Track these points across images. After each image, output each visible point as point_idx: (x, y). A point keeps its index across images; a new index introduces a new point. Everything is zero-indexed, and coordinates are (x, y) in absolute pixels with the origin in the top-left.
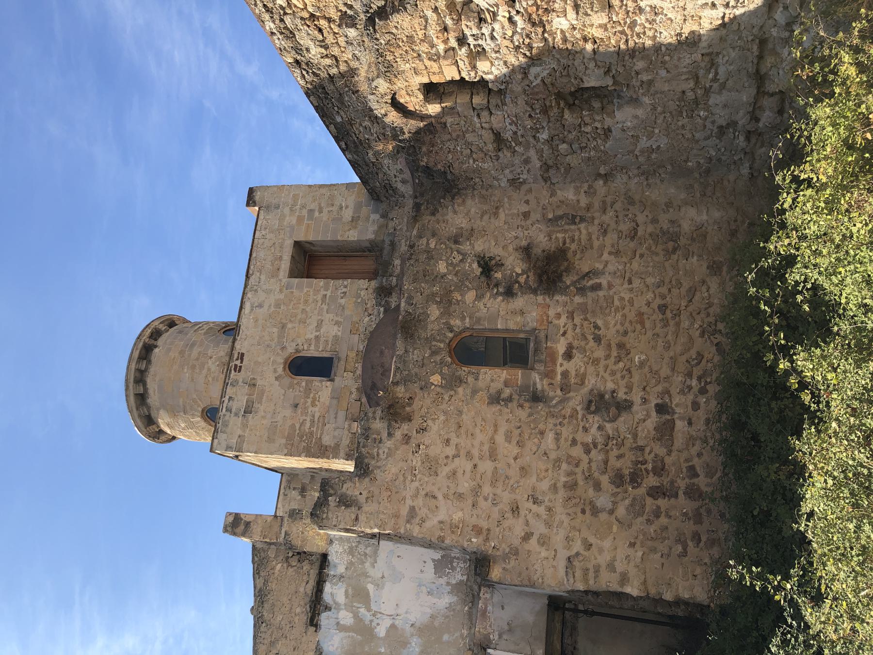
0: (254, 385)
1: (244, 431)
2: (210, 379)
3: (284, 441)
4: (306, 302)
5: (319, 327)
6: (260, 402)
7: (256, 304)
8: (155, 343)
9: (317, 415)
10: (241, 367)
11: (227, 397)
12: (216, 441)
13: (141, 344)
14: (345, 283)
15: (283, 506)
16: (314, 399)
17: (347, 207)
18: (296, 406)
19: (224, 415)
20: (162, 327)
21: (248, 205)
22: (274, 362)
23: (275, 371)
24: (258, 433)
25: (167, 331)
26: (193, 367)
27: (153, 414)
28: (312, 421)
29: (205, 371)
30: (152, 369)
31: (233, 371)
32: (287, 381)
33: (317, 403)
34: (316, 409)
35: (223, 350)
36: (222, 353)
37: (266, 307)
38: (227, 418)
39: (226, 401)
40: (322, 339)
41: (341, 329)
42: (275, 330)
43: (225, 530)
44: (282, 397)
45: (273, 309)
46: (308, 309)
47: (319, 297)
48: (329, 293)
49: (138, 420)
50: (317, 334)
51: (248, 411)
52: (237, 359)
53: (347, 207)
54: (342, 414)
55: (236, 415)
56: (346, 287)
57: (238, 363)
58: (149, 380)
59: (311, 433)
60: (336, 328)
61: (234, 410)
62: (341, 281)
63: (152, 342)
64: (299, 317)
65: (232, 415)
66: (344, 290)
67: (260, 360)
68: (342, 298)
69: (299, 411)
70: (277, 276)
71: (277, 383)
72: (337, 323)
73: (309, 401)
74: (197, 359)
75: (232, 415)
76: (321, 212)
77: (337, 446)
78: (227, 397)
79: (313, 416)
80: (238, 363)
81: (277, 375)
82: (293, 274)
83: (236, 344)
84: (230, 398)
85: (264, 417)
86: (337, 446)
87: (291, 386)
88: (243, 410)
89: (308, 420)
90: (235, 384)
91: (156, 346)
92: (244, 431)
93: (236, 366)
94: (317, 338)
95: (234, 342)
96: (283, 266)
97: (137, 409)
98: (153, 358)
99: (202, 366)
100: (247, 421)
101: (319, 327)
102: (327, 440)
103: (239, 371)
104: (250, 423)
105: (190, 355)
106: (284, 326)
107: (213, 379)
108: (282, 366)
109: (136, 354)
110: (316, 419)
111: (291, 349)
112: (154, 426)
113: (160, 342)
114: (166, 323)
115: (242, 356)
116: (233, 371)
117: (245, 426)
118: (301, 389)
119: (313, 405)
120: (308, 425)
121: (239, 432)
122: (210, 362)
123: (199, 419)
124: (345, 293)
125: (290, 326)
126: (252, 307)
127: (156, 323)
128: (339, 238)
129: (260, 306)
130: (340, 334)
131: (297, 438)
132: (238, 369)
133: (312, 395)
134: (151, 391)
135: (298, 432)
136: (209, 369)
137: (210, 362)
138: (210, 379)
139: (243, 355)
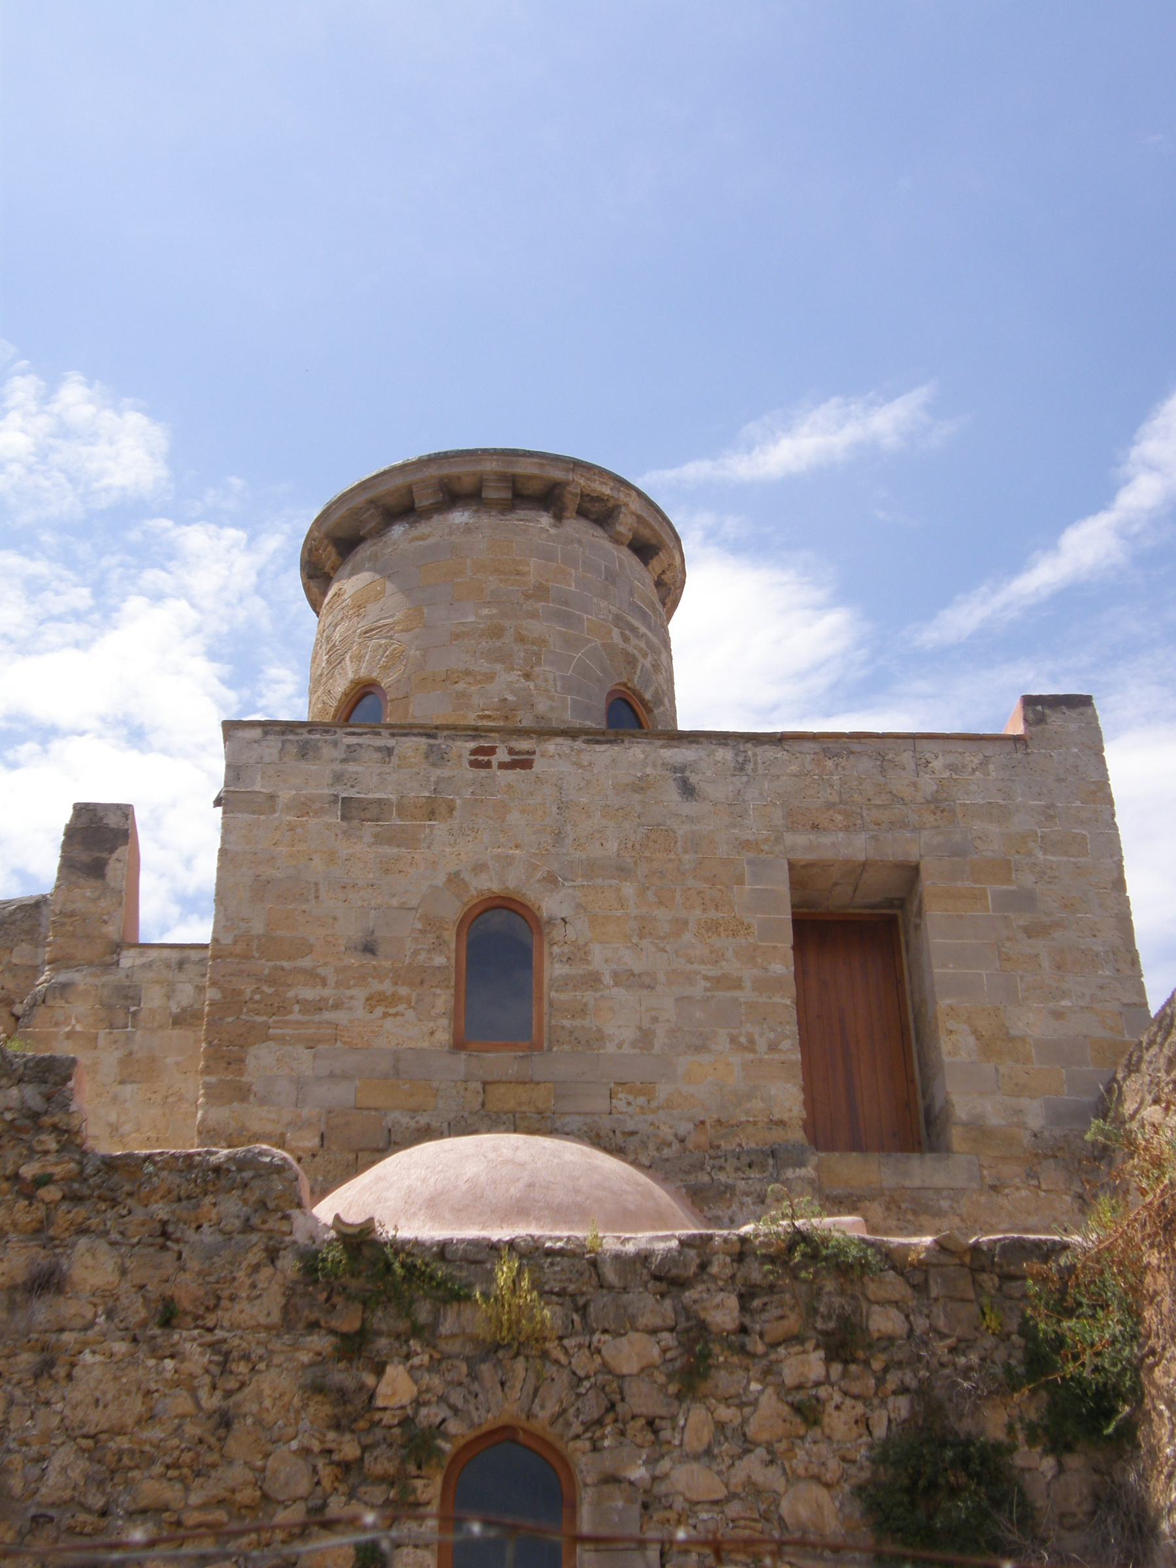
0: (432, 815)
1: (288, 808)
2: (461, 686)
3: (258, 927)
4: (713, 927)
5: (628, 979)
6: (378, 839)
7: (693, 779)
8: (570, 512)
9: (340, 1016)
10: (488, 765)
11: (391, 742)
12: (257, 733)
13: (557, 474)
14: (786, 1044)
15: (148, 966)
16: (394, 999)
17: (1058, 1015)
18: (369, 948)
19: (335, 744)
20: (625, 525)
21: (1029, 702)
22: (508, 861)
23: (479, 868)
24: (283, 849)
25: (616, 540)
26: (496, 632)
27: (364, 551)
28: (318, 1006)
29: (483, 666)
30: (487, 521)
31: (472, 745)
32: (452, 911)
33: (379, 1011)
34: (360, 1013)
35: (553, 701)
36: (542, 707)
37: (688, 808)
38: (327, 751)
39: (379, 742)
40: (589, 996)
41: (627, 1049)
42: (613, 846)
43: (125, 811)
44: (394, 902)
45: (682, 830)
46: (687, 937)
47: (732, 966)
48: (746, 995)
49: (342, 511)
50: (607, 979)
51: (350, 808)
52: (511, 751)
53: (1058, 1015)
54: (342, 1094)
55: (338, 778)
56: (773, 1047)
57: (502, 755)
58: (459, 517)
59: (283, 1009)
60: (629, 1034)
61: (352, 767)
62: (792, 1028)
63: (572, 504)
64: (660, 913)
65: (337, 767)
66: (761, 1045)
67: (514, 817)
68: (733, 1040)
69: (353, 960)
70: (792, 828)
71: (440, 880)
72: (645, 1038)
73: (386, 987)
74: (521, 639)
75: (337, 767)
76: (1030, 932)
77: (242, 1093)
78: (391, 742)
79: (337, 1006)
80: (502, 755)
81: (465, 875)
82: (801, 876)
83: (560, 740)
84: (389, 751)
85: (332, 857)
86: (242, 1093)
87: (431, 924)
88: (352, 793)
89: (326, 992)
90: (436, 757)
91: (559, 517)
92: (288, 808)
93: (491, 751)
94: (593, 980)
95: (571, 734)
96: (826, 840)
97: (371, 502)
98: (522, 514)
99: (503, 657)
100: (319, 812)
101: (628, 979)
102: (262, 1060)
103: (475, 764)
104: (313, 822)
105: (533, 615)
106: (624, 872)
107: (463, 695)
108: (496, 887)
109: (524, 468)
110: (327, 1016)
111: (550, 905)
112: (334, 556)
113: (575, 527)
114: (645, 533)
115: (522, 763)
116: (472, 745)
117: (304, 807)
118: (422, 956)
119: (373, 1001)
120: (309, 993)
121: (285, 795)
122: (515, 676)
123: (351, 676)
124: (751, 1046)
125: (629, 889)
126: (682, 769)
127: (635, 505)
128: (943, 1003)
129: (688, 790)
130: (610, 1048)
131: (265, 966)
132: (481, 759)
133: (403, 991)
134: (423, 528)
135: (286, 964)
136: (490, 677)
137: (515, 676)
138: (461, 686)
139: (526, 764)
